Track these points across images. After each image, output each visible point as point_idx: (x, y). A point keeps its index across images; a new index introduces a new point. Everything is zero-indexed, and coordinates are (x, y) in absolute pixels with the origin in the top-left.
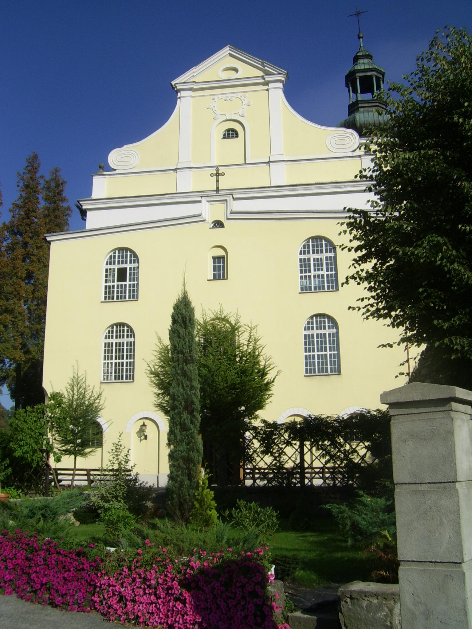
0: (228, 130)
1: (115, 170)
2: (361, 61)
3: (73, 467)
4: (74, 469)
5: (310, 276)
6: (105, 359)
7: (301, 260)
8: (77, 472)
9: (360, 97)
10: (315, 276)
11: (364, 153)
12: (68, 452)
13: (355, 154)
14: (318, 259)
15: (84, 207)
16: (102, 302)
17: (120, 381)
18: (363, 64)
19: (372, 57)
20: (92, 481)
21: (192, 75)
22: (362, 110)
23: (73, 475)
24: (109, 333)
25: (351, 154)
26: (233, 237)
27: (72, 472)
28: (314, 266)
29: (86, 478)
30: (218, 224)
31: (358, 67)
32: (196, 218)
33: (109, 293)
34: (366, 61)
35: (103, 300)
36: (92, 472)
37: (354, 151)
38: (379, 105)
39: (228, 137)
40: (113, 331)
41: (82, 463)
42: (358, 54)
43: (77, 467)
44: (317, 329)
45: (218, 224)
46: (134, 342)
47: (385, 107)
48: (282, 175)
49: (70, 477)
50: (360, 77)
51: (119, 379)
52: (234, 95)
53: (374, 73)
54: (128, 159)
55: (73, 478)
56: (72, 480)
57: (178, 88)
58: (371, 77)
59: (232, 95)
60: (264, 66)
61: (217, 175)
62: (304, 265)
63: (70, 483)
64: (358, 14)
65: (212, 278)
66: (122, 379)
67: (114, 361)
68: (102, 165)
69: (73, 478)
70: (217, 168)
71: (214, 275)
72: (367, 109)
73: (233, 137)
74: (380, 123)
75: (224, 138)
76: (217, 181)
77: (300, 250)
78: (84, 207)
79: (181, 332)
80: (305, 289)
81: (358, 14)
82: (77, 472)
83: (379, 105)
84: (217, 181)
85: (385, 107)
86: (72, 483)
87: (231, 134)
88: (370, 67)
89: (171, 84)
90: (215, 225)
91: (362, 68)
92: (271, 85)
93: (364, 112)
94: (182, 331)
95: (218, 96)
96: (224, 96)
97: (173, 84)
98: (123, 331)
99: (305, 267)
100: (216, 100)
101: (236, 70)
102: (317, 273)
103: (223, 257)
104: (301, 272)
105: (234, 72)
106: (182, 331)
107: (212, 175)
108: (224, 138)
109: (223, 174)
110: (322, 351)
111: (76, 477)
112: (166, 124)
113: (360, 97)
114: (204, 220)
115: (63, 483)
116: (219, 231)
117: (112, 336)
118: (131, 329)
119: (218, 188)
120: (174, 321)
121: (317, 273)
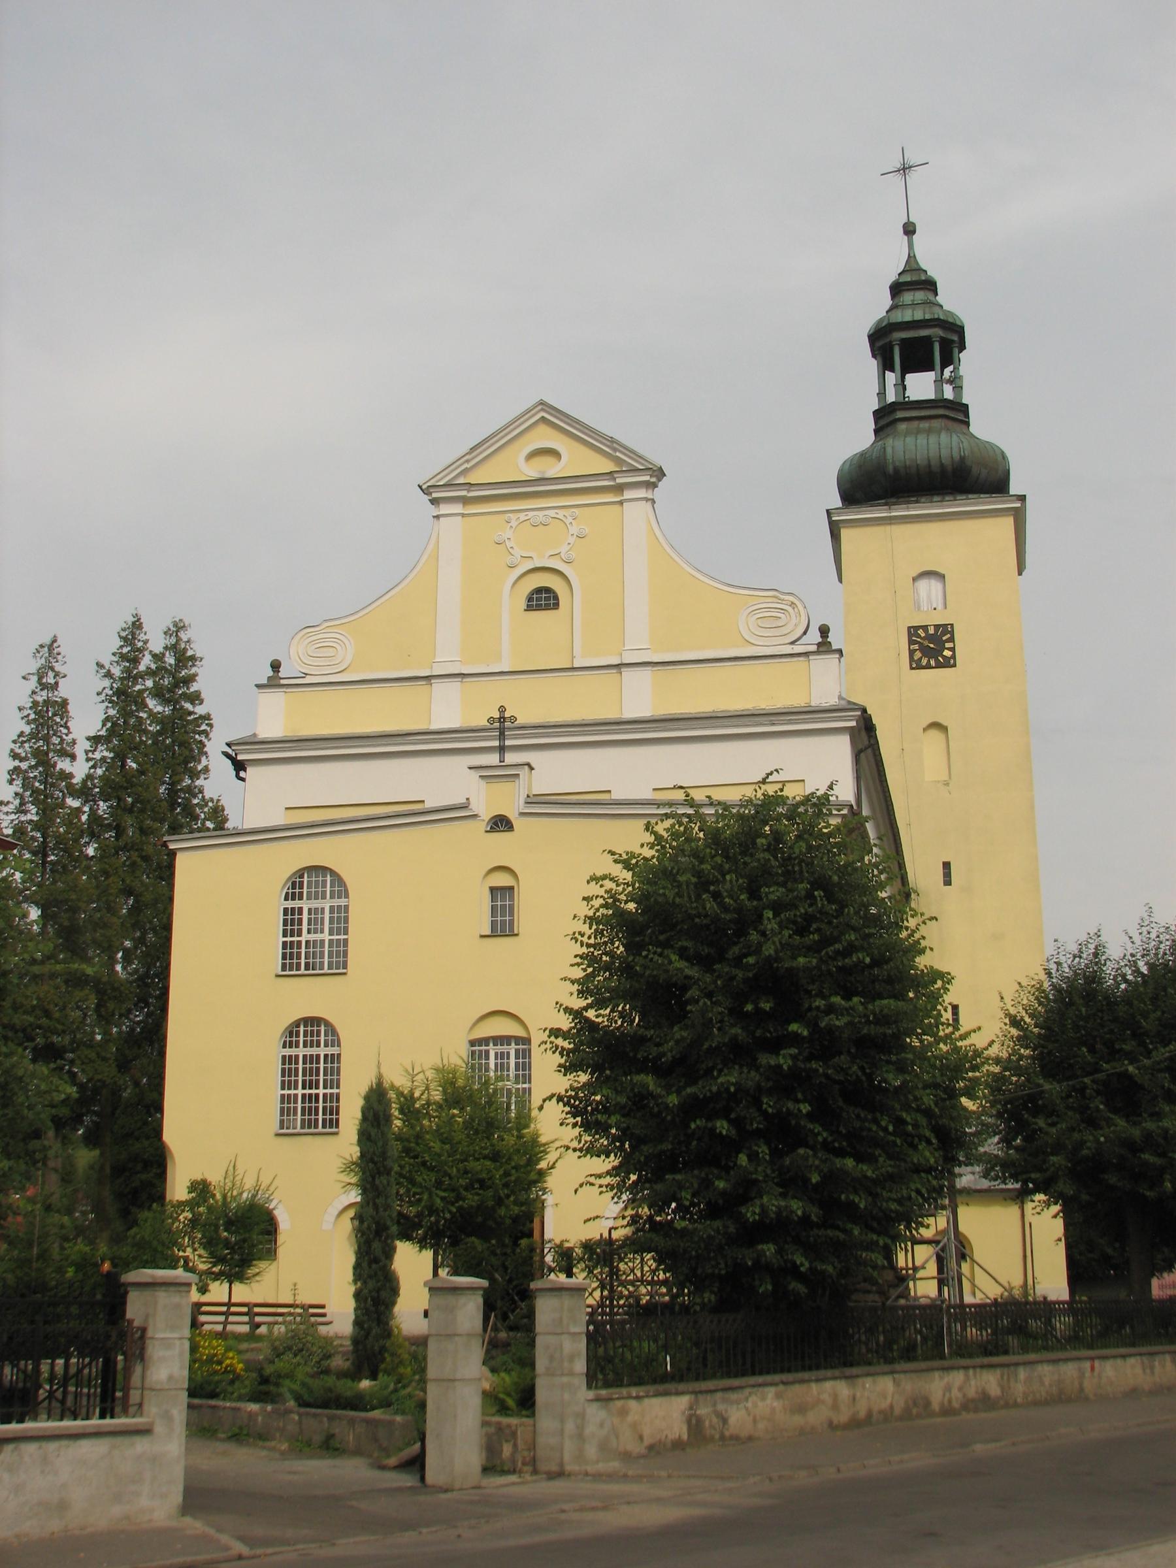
0: (539, 591)
2: (907, 297)
3: (226, 1300)
4: (229, 1304)
6: (283, 1088)
8: (233, 1309)
11: (814, 648)
12: (217, 1277)
13: (798, 649)
17: (312, 1130)
20: (258, 1325)
22: (902, 426)
23: (227, 1314)
24: (294, 887)
25: (788, 650)
27: (224, 1309)
29: (246, 1319)
30: (501, 824)
36: (257, 1310)
38: (947, 413)
39: (539, 608)
40: (301, 883)
41: (242, 1293)
43: (233, 1300)
45: (501, 824)
46: (339, 1055)
48: (639, 698)
49: (222, 1318)
50: (904, 342)
51: (309, 1127)
52: (552, 513)
53: (936, 332)
54: (331, 652)
55: (227, 1319)
56: (225, 1323)
58: (928, 341)
59: (546, 512)
63: (220, 1328)
64: (905, 169)
65: (488, 932)
66: (316, 1127)
67: (300, 1092)
69: (227, 1319)
72: (915, 424)
73: (547, 608)
74: (942, 465)
75: (529, 608)
79: (373, 1134)
81: (905, 169)
82: (233, 1309)
83: (947, 413)
86: (224, 1328)
87: (543, 599)
88: (928, 317)
90: (496, 824)
91: (908, 318)
92: (628, 494)
93: (907, 433)
94: (373, 1132)
96: (531, 514)
98: (319, 1032)
100: (514, 524)
101: (554, 453)
103: (511, 888)
105: (548, 460)
106: (373, 1132)
111: (231, 1319)
114: (475, 816)
115: (207, 1327)
117: (301, 894)
118: (331, 1030)
120: (365, 1118)
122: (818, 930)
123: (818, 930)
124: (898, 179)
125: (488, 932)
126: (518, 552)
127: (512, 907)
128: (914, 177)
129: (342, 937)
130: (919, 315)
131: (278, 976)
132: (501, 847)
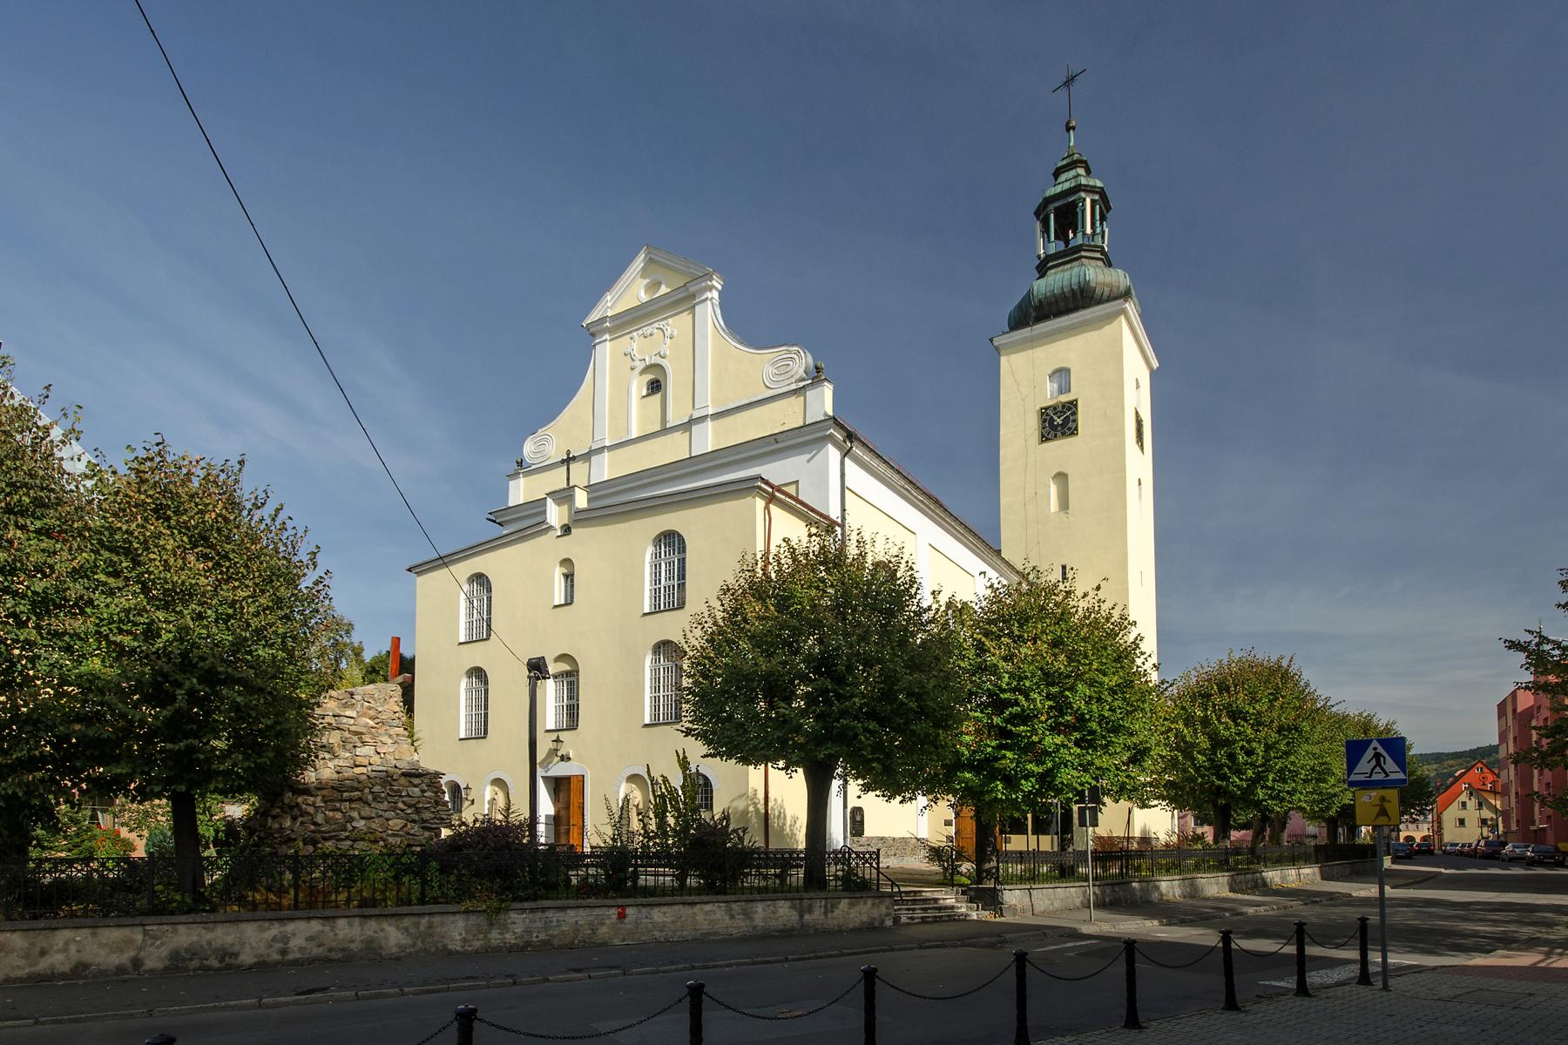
2: (1063, 177)
25: (794, 387)
48: (708, 439)
128: (1075, 87)
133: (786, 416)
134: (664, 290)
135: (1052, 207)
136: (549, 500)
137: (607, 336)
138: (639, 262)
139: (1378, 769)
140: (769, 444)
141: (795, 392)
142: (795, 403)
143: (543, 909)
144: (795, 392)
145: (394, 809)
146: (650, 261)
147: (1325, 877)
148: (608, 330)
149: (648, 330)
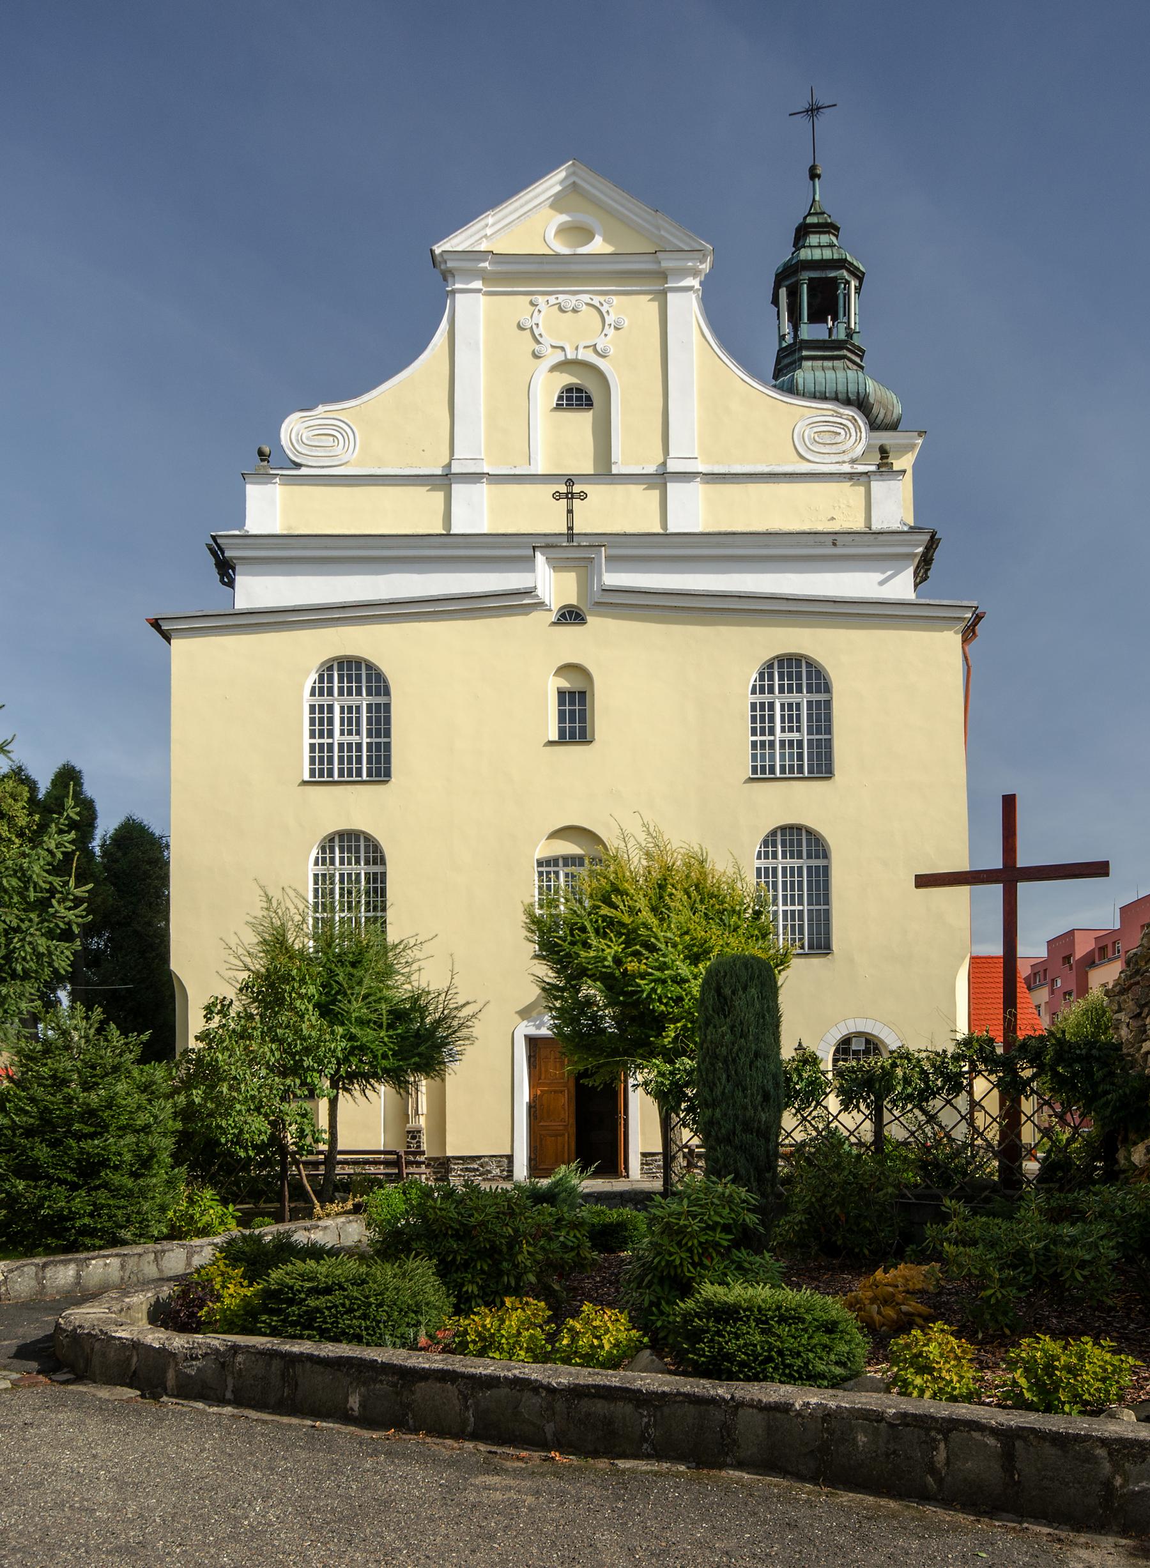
0: (569, 390)
1: (298, 466)
2: (813, 239)
5: (772, 743)
7: (753, 706)
9: (808, 331)
10: (782, 742)
11: (873, 468)
14: (790, 705)
15: (227, 554)
16: (305, 783)
18: (817, 248)
19: (837, 229)
21: (482, 233)
22: (807, 364)
25: (846, 468)
26: (603, 645)
28: (783, 721)
30: (571, 616)
31: (805, 254)
32: (519, 602)
33: (321, 762)
34: (825, 239)
35: (307, 777)
37: (853, 461)
42: (809, 220)
44: (809, 857)
47: (858, 360)
48: (693, 511)
57: (450, 264)
60: (658, 228)
61: (570, 496)
62: (761, 717)
64: (813, 110)
65: (556, 738)
68: (267, 450)
70: (570, 481)
71: (562, 732)
72: (819, 363)
75: (559, 407)
76: (570, 511)
77: (752, 683)
78: (227, 554)
80: (762, 773)
81: (813, 110)
83: (849, 354)
84: (570, 511)
85: (858, 360)
89: (432, 251)
90: (563, 616)
95: (547, 298)
97: (438, 251)
99: (321, 723)
102: (788, 736)
103: (583, 694)
104: (754, 733)
107: (557, 496)
108: (559, 407)
109: (583, 496)
110: (793, 904)
112: (422, 357)
113: (808, 331)
116: (570, 632)
119: (570, 528)
121: (788, 736)
122: (49, 1207)
123: (49, 1207)
124: (803, 122)
125: (556, 738)
126: (547, 340)
127: (583, 713)
128: (823, 119)
129: (382, 740)
130: (827, 254)
131: (305, 783)
132: (574, 644)
133: (835, 509)
134: (598, 245)
135: (806, 275)
136: (540, 558)
137: (477, 284)
138: (553, 183)
139: (989, 1120)
140: (822, 544)
141: (851, 476)
142: (853, 494)
143: (107, 1257)
144: (851, 476)
145: (339, 1064)
146: (572, 188)
147: (288, 1234)
148: (484, 276)
149: (570, 301)
